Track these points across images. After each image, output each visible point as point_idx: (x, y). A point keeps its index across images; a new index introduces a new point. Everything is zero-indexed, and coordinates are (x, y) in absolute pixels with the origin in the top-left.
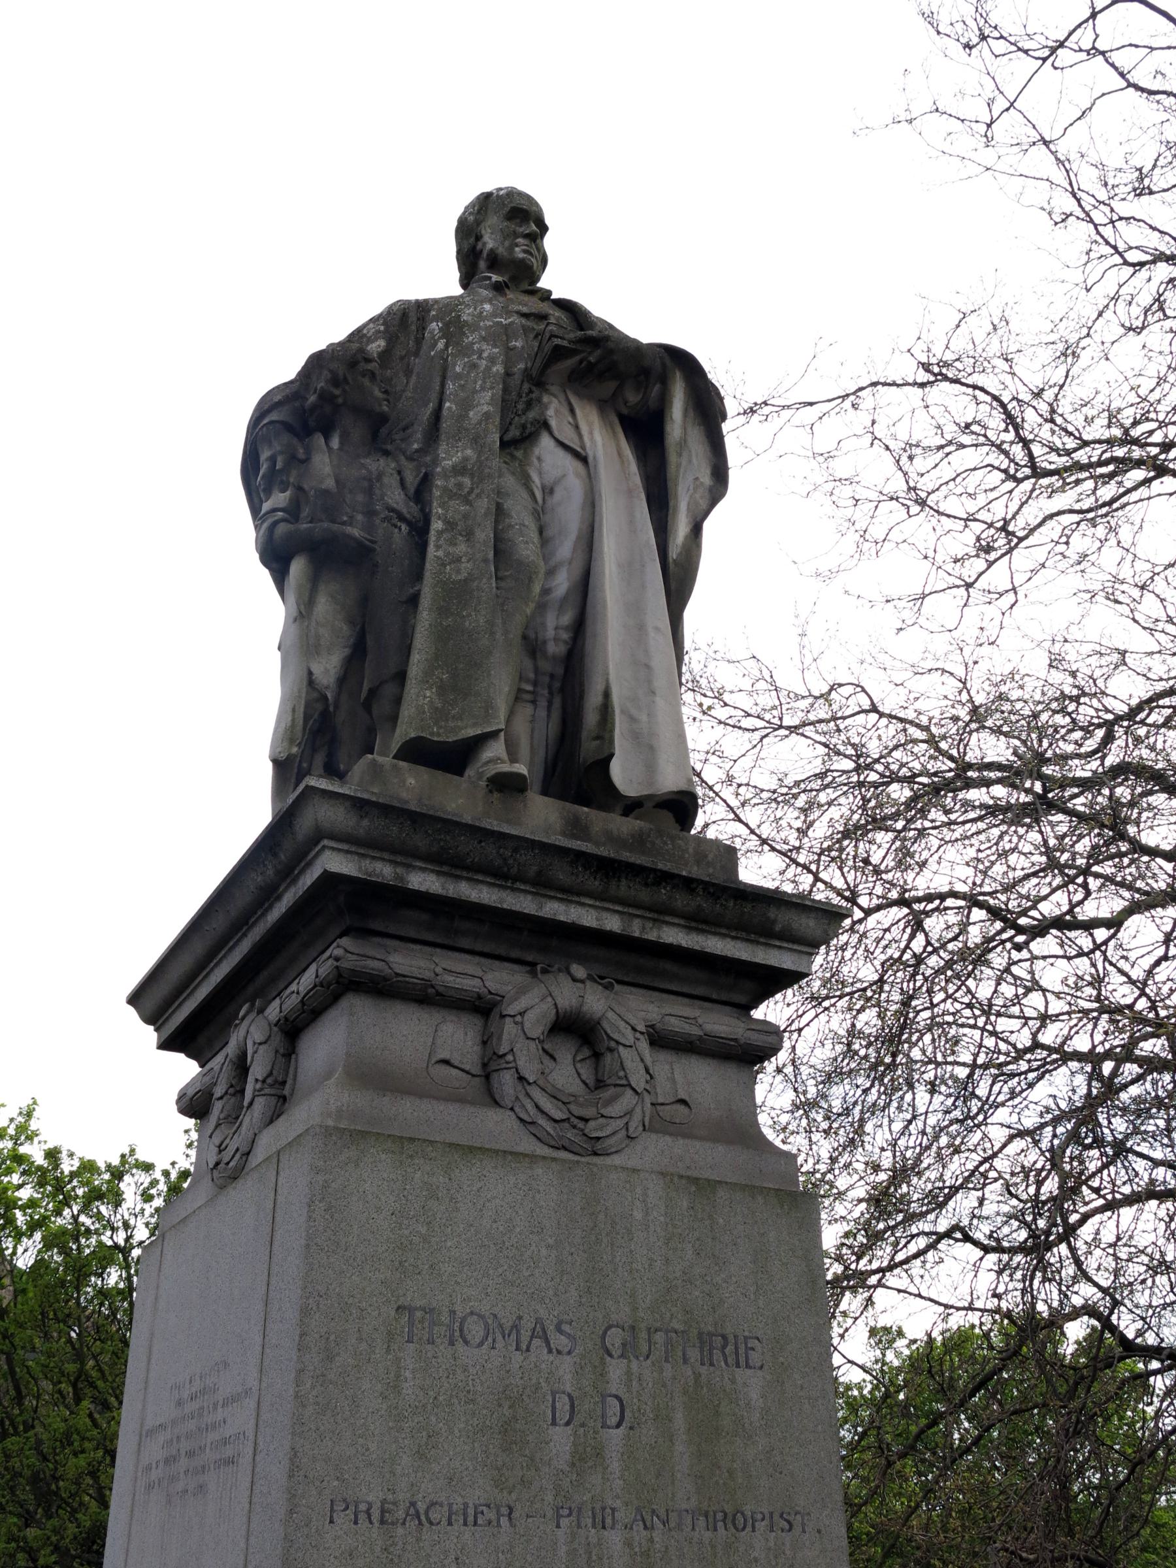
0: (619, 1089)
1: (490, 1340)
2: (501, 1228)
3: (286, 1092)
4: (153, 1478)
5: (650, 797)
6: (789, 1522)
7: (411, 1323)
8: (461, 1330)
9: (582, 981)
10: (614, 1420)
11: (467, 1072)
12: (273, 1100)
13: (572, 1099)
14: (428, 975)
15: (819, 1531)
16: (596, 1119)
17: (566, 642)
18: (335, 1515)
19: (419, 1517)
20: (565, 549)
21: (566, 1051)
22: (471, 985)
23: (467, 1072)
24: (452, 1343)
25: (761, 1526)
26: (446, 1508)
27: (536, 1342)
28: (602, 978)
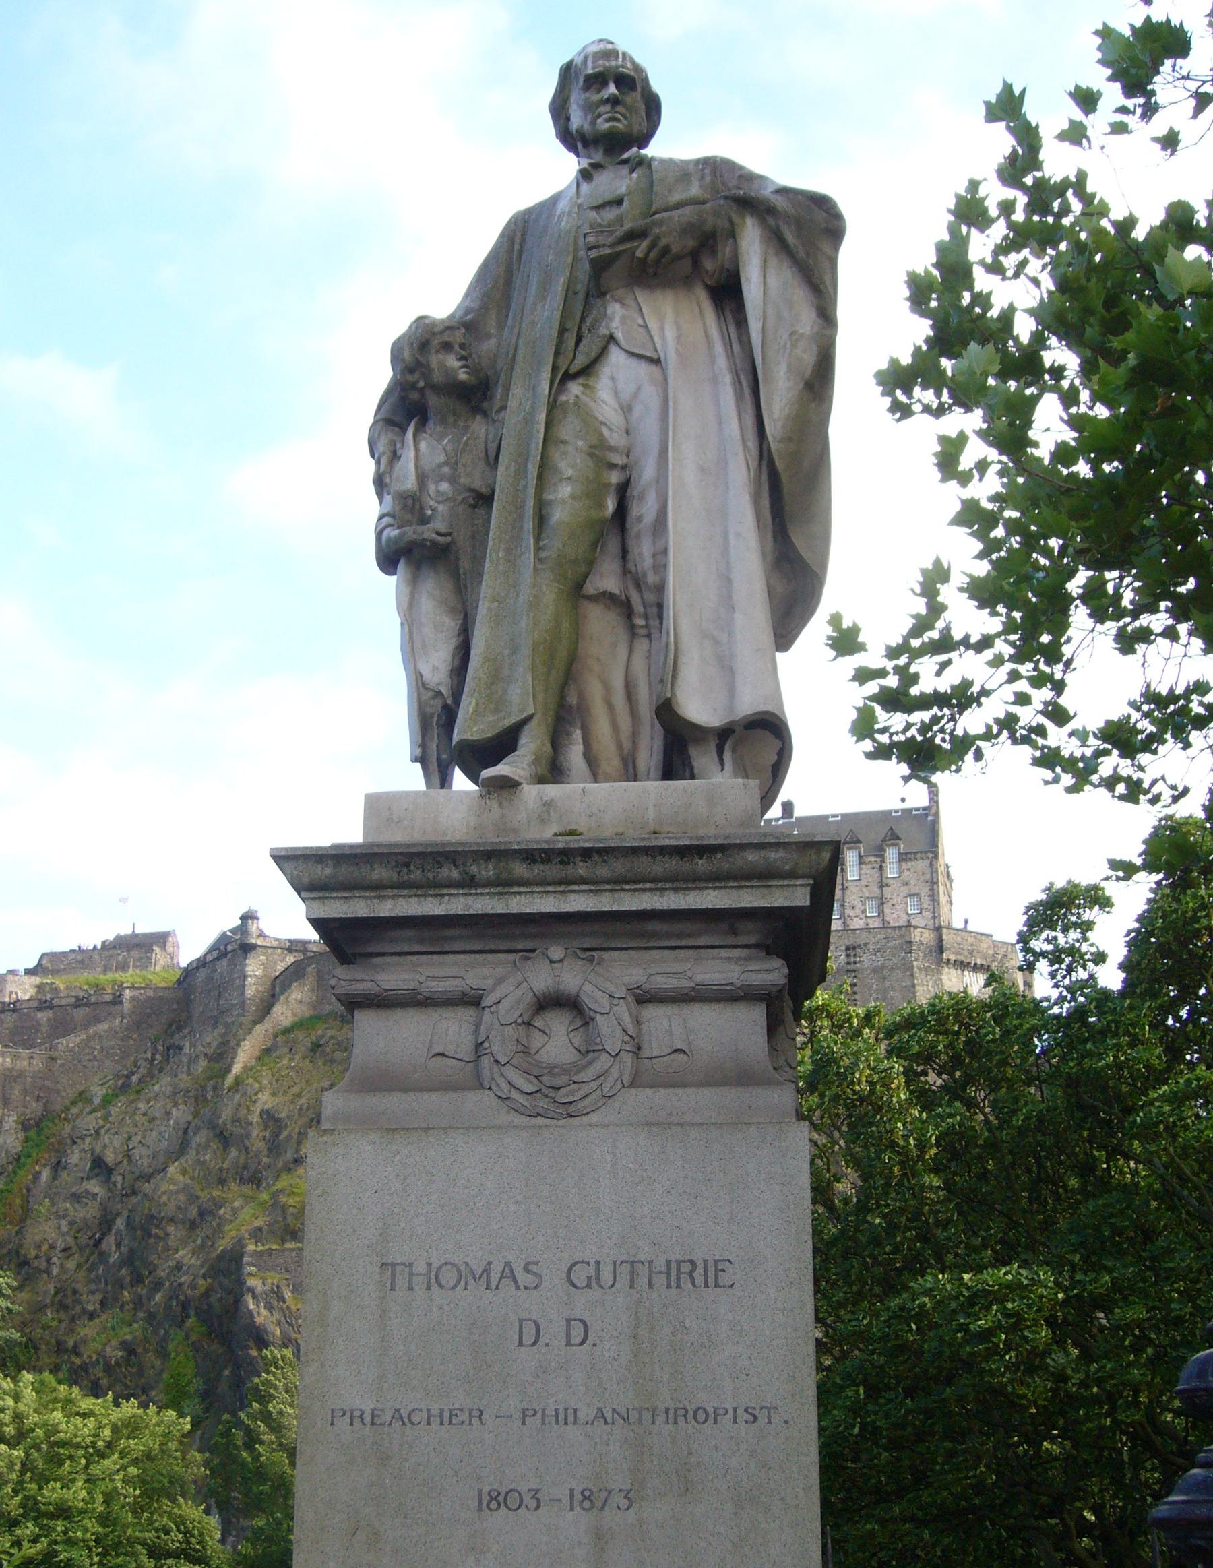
0: (597, 1054)
1: (463, 1283)
7: (393, 1275)
10: (578, 1340)
14: (412, 985)
22: (452, 986)
24: (429, 1288)
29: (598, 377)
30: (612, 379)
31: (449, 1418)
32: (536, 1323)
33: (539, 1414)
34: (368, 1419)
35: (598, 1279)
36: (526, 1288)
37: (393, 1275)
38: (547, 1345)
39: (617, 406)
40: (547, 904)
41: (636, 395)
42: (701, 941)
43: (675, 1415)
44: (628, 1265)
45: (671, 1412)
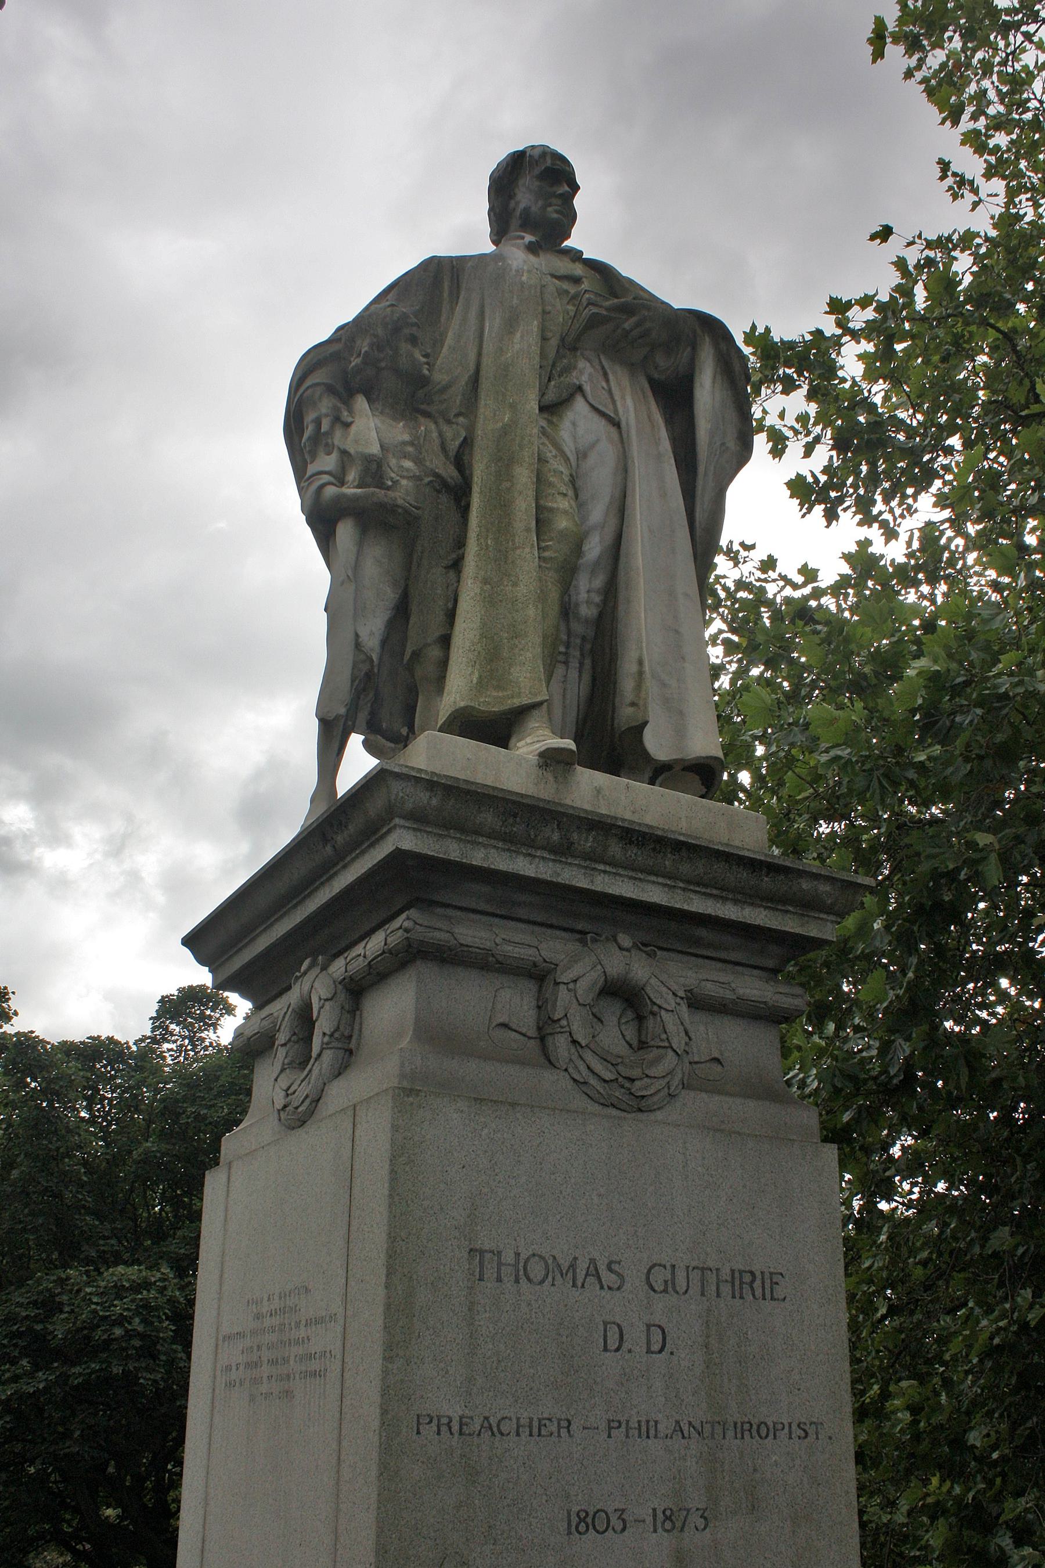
1: (550, 1278)
2: (559, 1179)
3: (353, 1045)
4: (233, 1377)
5: (676, 761)
6: (804, 1430)
7: (481, 1264)
8: (525, 1269)
9: (628, 950)
10: (656, 1347)
11: (524, 1035)
12: (341, 1053)
13: (620, 1060)
14: (488, 945)
15: (830, 1438)
16: (641, 1079)
17: (598, 605)
18: (421, 1427)
19: (493, 1429)
20: (597, 512)
21: (612, 1011)
23: (524, 1035)
24: (517, 1281)
25: (783, 1434)
26: (514, 1421)
27: (591, 1280)
28: (645, 945)
29: (561, 417)
30: (574, 424)
31: (537, 1428)
32: (619, 1326)
33: (624, 1425)
34: (456, 1428)
35: (673, 1284)
36: (610, 1288)
37: (481, 1264)
38: (630, 1351)
39: (573, 449)
40: (624, 888)
41: (593, 446)
42: (734, 956)
43: (747, 1429)
44: (700, 1272)
45: (739, 1425)
